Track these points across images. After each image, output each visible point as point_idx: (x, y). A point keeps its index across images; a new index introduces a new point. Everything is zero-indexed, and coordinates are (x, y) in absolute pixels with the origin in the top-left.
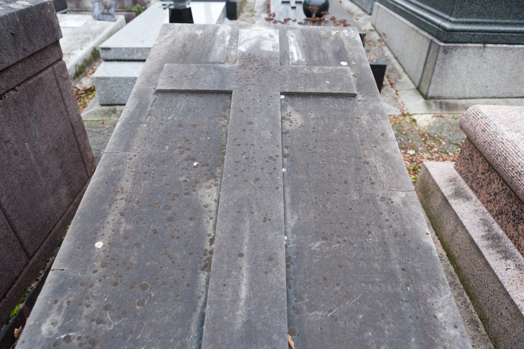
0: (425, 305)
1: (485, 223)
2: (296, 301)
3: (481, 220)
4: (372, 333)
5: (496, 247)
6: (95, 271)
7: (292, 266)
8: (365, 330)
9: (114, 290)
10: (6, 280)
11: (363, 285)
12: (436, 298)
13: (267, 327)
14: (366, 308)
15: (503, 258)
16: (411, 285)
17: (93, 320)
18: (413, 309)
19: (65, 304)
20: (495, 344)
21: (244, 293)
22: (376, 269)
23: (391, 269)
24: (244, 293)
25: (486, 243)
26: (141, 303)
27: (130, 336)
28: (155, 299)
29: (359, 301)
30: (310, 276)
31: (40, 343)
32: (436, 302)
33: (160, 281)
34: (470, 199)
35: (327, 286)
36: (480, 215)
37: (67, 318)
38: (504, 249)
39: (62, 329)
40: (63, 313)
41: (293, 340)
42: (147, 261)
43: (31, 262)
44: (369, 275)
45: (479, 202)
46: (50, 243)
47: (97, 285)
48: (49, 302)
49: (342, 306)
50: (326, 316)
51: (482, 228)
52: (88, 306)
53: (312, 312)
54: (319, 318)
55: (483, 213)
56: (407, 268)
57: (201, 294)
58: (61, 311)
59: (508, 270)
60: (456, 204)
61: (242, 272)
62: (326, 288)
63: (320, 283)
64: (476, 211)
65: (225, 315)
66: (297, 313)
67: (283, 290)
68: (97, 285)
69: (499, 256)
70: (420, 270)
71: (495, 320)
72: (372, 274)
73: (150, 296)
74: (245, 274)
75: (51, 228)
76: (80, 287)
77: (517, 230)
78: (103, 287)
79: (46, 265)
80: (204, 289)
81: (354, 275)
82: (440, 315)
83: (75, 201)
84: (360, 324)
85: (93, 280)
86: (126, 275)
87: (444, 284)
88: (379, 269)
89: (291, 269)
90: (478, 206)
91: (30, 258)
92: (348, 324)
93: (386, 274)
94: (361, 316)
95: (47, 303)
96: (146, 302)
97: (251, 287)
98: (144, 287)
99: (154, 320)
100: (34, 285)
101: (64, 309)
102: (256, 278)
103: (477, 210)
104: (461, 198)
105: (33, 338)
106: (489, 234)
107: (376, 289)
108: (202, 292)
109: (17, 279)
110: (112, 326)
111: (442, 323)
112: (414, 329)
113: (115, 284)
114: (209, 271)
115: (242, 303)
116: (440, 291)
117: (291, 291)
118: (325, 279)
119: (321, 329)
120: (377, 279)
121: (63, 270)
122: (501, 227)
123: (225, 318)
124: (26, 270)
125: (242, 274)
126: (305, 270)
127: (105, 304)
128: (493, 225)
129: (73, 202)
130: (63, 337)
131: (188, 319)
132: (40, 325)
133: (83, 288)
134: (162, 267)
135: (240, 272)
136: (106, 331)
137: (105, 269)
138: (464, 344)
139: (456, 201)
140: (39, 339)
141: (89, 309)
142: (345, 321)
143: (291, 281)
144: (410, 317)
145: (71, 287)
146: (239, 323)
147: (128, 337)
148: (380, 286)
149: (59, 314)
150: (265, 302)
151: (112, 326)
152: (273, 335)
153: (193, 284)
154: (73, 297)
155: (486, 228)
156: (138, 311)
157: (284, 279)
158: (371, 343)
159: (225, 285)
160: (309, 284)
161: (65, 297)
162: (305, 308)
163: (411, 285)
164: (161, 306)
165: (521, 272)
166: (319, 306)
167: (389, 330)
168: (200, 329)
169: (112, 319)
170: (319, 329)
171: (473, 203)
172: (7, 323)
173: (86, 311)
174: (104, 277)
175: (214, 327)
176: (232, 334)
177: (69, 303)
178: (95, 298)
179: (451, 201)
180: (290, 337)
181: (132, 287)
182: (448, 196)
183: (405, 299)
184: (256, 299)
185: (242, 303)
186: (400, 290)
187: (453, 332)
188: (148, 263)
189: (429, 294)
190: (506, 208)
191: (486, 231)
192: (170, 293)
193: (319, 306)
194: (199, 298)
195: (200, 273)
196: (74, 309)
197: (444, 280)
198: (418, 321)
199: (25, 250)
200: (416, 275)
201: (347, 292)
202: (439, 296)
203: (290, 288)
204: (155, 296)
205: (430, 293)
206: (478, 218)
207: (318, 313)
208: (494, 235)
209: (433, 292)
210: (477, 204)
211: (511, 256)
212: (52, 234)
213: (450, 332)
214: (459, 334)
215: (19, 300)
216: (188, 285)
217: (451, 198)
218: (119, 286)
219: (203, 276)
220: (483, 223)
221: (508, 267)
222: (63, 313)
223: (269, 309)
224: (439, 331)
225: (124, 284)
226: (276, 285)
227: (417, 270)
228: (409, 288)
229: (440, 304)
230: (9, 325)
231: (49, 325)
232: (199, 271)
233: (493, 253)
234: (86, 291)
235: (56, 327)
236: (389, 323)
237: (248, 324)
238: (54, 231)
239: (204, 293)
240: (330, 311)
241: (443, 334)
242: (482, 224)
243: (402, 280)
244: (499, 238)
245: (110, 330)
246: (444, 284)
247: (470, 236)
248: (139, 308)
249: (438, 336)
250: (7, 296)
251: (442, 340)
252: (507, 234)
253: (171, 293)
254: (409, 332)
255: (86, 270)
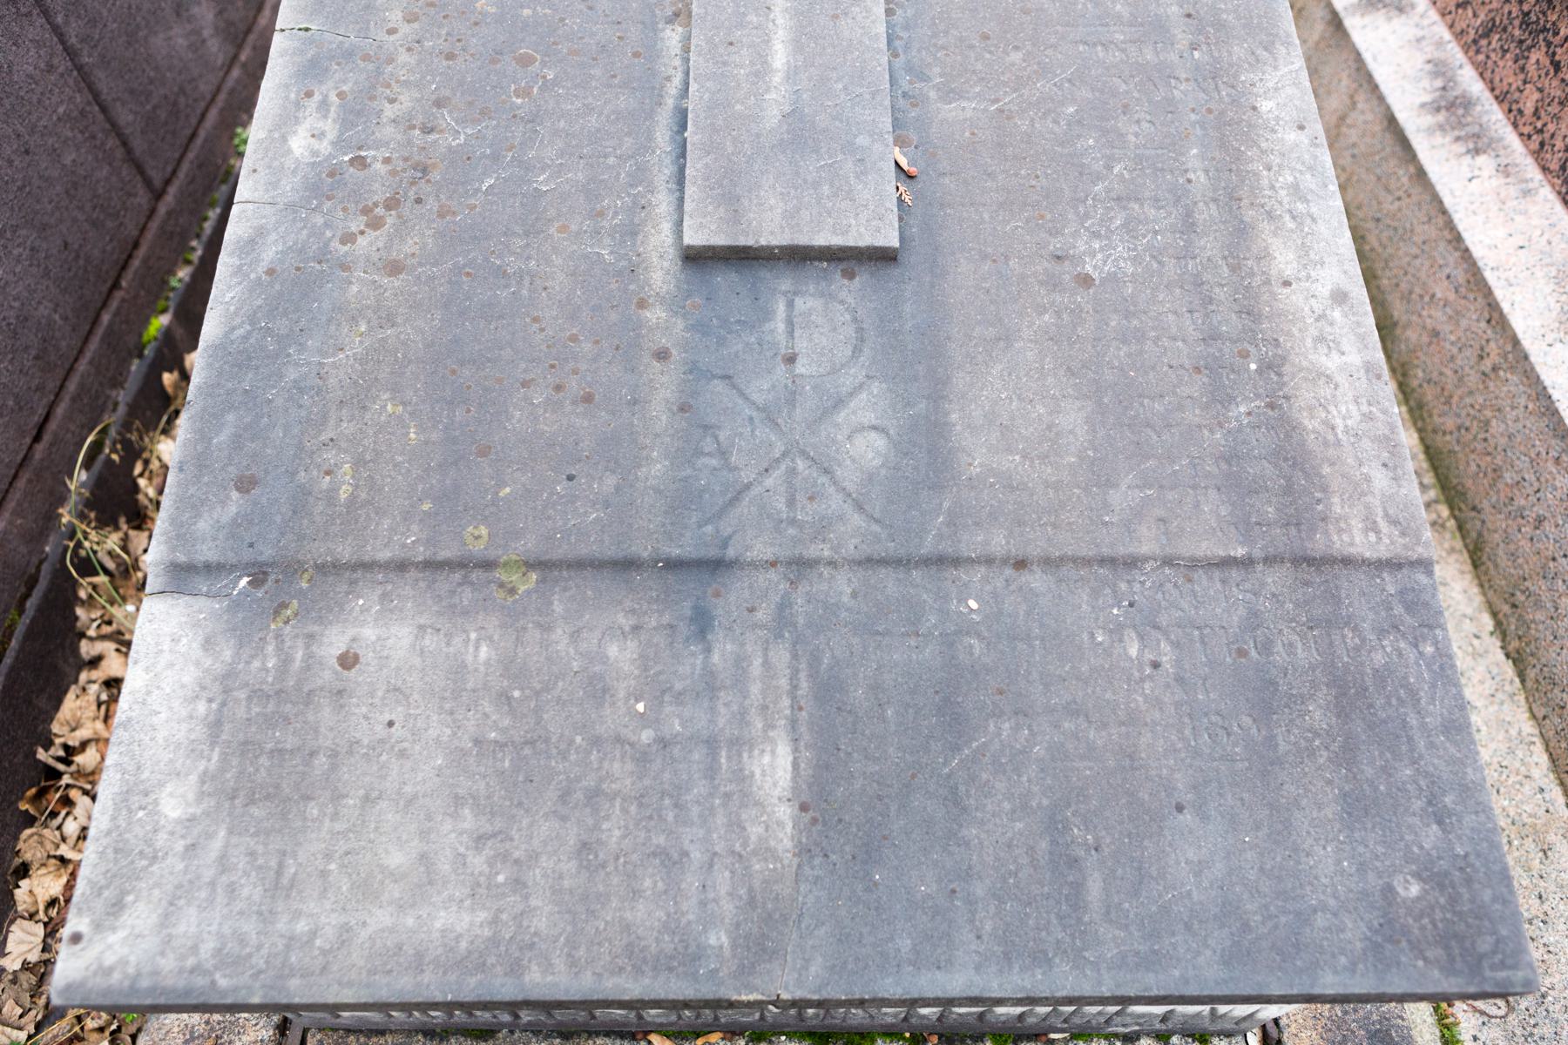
0: (1233, 87)
1: (1439, 69)
2: (910, 82)
3: (1429, 62)
4: (1096, 141)
5: (1453, 129)
6: (391, 31)
7: (899, 12)
8: (1079, 136)
9: (449, 68)
10: (111, 240)
11: (1081, 48)
12: (1263, 73)
13: (842, 122)
14: (1085, 93)
15: (1468, 152)
16: (1204, 48)
17: (413, 127)
18: (1202, 95)
19: (333, 98)
20: (1401, 379)
21: (780, 57)
22: (1119, 16)
23: (1156, 15)
24: (780, 57)
25: (1429, 120)
26: (525, 93)
27: (510, 154)
28: (556, 82)
29: (1069, 81)
30: (946, 32)
31: (294, 172)
32: (1261, 80)
33: (564, 48)
34: (1408, 9)
35: (990, 52)
36: (1428, 49)
37: (346, 123)
38: (1476, 129)
39: (339, 144)
40: (332, 114)
41: (905, 155)
42: (522, 7)
43: (162, 209)
44: (1099, 28)
45: (1433, 15)
46: (200, 166)
47: (403, 57)
48: (293, 96)
49: (1026, 92)
50: (985, 110)
51: (1426, 83)
52: (392, 101)
53: (950, 103)
54: (969, 114)
55: (1440, 44)
56: (1197, 12)
57: (671, 71)
58: (328, 111)
59: (1474, 181)
60: (1364, 27)
61: (772, 16)
62: (988, 56)
63: (972, 47)
64: (1419, 40)
65: (737, 102)
66: (914, 105)
67: (879, 51)
68: (403, 57)
69: (1460, 148)
70: (1230, 18)
71: (1414, 318)
72: (1107, 25)
73: (544, 77)
74: (780, 21)
75: (194, 121)
76: (362, 64)
77: (1522, 69)
78: (419, 62)
79: (201, 228)
80: (677, 62)
81: (1059, 28)
82: (1266, 106)
83: (243, 57)
84: (1069, 125)
85: (392, 49)
86: (473, 36)
87: (1288, 44)
88: (1126, 14)
89: (898, 17)
90: (1429, 26)
91: (158, 195)
92: (1037, 126)
93: (1142, 25)
94: (1071, 110)
95: (287, 98)
96: (535, 90)
97: (797, 46)
98: (526, 61)
99: (562, 124)
100: (184, 273)
101: (333, 109)
102: (809, 29)
103: (1423, 38)
104: (1384, 11)
105: (276, 163)
106: (1442, 97)
107: (1114, 56)
108: (675, 68)
109: (136, 245)
110: (462, 137)
111: (1268, 119)
112: (1199, 132)
113: (450, 56)
114: (688, 24)
115: (777, 79)
116: (1276, 60)
117: (899, 62)
118: (986, 37)
119: (973, 134)
120: (1117, 36)
121: (307, 30)
122: (1481, 75)
123: (738, 107)
124: (154, 225)
125: (773, 21)
126: (933, 18)
127: (433, 97)
128: (1460, 72)
129: (235, 57)
130: (346, 158)
131: (646, 119)
132: (284, 139)
133: (371, 67)
134: (562, 20)
135: (768, 16)
136: (450, 148)
137: (416, 25)
138: (1316, 157)
139: (1368, 19)
140: (290, 164)
141: (396, 106)
142: (1032, 120)
143: (897, 43)
144: (1193, 110)
145: (338, 64)
146: (772, 116)
147: (505, 157)
148: (1123, 51)
149: (325, 117)
150: (834, 75)
151: (462, 137)
152: (855, 136)
153: (649, 52)
154: (350, 85)
155: (1439, 83)
156: (519, 108)
157: (881, 29)
158: (1093, 159)
159: (731, 44)
160: (943, 48)
161: (330, 84)
162: (933, 94)
163: (1204, 48)
164: (575, 96)
165: (1508, 180)
166: (968, 92)
167: (1136, 135)
168: (678, 138)
169: (456, 122)
170: (967, 134)
171: (1416, 19)
172: (140, 356)
173: (389, 111)
174: (418, 42)
175: (712, 124)
176: (758, 136)
177: (341, 95)
178: (406, 84)
179: (1352, 23)
180: (897, 149)
181: (494, 61)
182: (1346, 9)
183: (1184, 76)
184: (812, 69)
185: (777, 79)
186: (1174, 57)
187: (1292, 136)
188: (527, 12)
189: (1246, 66)
190: (1506, 11)
191: (1437, 90)
192: (592, 72)
193: (968, 92)
194: (668, 79)
195: (663, 30)
196: (358, 107)
197: (1288, 35)
198: (1211, 116)
199: (140, 169)
200: (1220, 25)
201: (1039, 63)
202: (1270, 69)
203: (896, 55)
204: (556, 77)
205: (1249, 63)
206: (1418, 60)
207: (964, 104)
208: (1456, 98)
209: (1258, 61)
210: (1426, 22)
211: (1489, 145)
212: (199, 141)
213: (1286, 136)
214: (1306, 141)
215: (154, 302)
216: (636, 55)
217: (1353, 14)
218: (460, 60)
219: (672, 37)
220: (1434, 69)
221: (1477, 173)
222: (332, 114)
223: (845, 88)
224: (1258, 135)
225: (472, 55)
226: (860, 42)
227: (1224, 16)
228: (1196, 54)
229: (1270, 84)
230: (148, 361)
231: (305, 138)
232: (660, 26)
233: (1443, 145)
234: (379, 72)
235: (325, 143)
236: (1138, 122)
237: (793, 115)
238: (202, 134)
239: (680, 69)
240: (997, 100)
241: (1267, 140)
242: (1430, 73)
243: (1182, 38)
244: (1467, 103)
245: (458, 145)
246: (1288, 44)
247: (1388, 108)
248: (519, 101)
249: (1256, 144)
250: (124, 284)
251: (1263, 152)
252: (1493, 90)
253: (596, 72)
254: (1186, 137)
255: (368, 29)
